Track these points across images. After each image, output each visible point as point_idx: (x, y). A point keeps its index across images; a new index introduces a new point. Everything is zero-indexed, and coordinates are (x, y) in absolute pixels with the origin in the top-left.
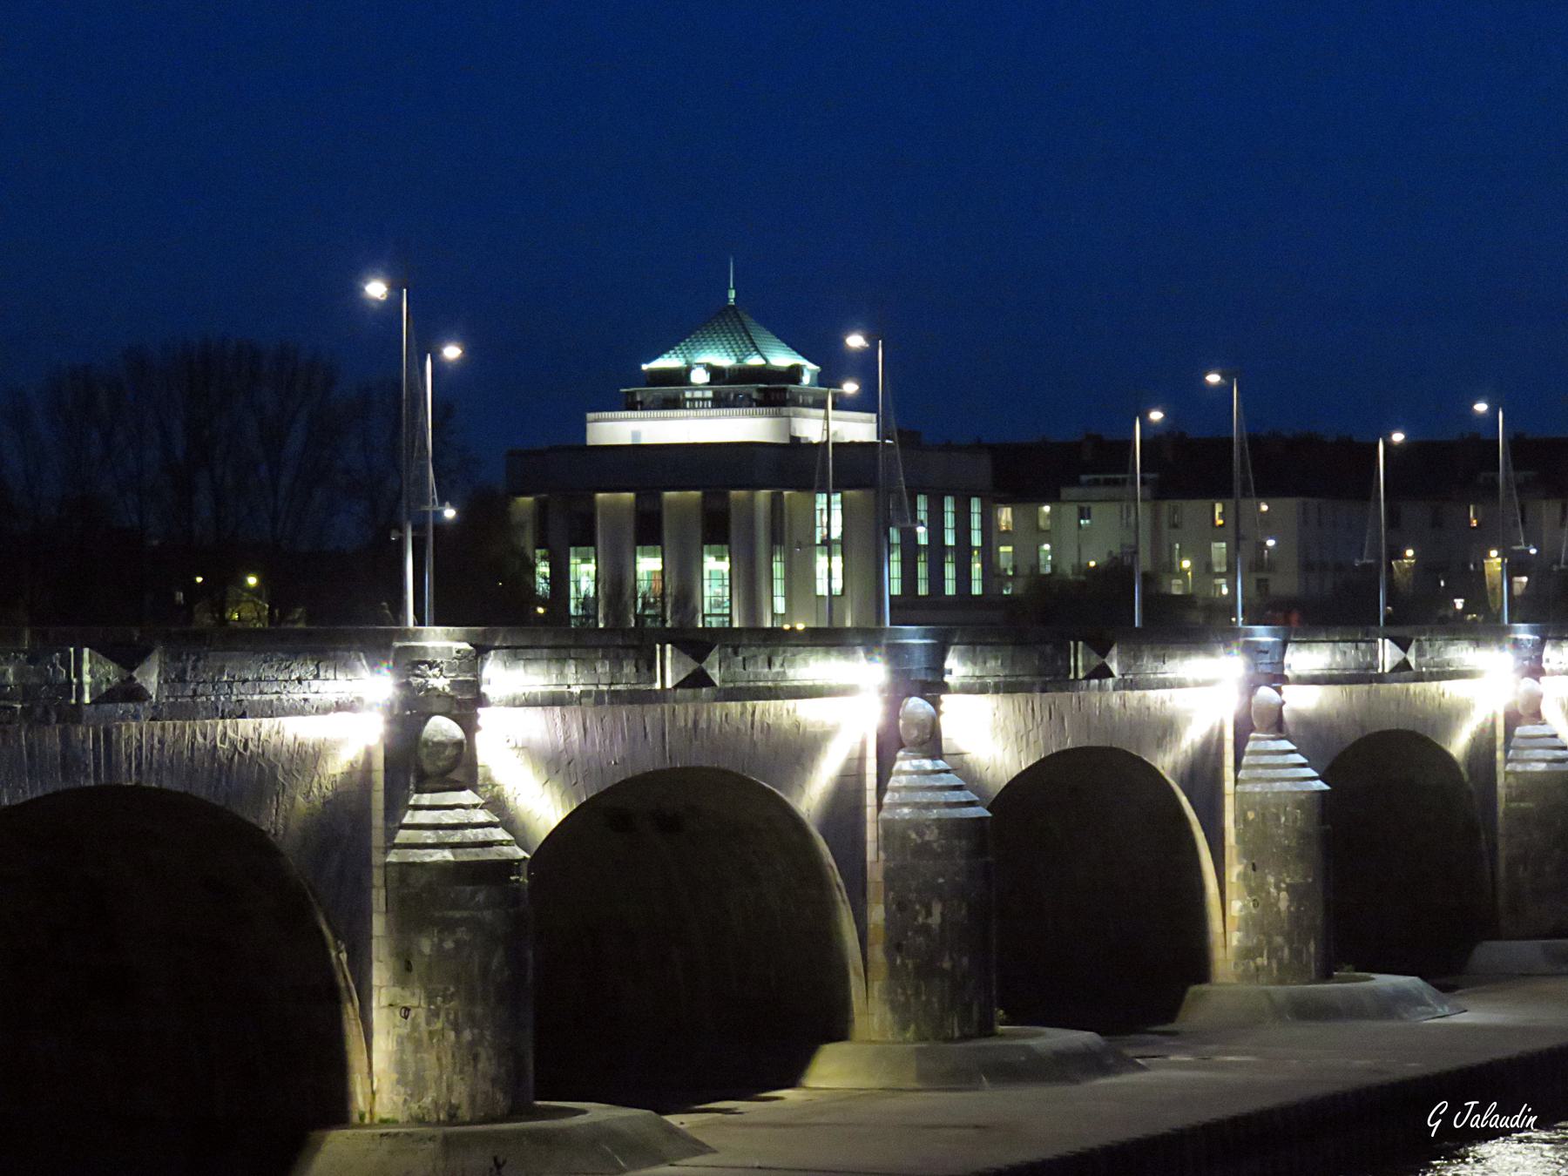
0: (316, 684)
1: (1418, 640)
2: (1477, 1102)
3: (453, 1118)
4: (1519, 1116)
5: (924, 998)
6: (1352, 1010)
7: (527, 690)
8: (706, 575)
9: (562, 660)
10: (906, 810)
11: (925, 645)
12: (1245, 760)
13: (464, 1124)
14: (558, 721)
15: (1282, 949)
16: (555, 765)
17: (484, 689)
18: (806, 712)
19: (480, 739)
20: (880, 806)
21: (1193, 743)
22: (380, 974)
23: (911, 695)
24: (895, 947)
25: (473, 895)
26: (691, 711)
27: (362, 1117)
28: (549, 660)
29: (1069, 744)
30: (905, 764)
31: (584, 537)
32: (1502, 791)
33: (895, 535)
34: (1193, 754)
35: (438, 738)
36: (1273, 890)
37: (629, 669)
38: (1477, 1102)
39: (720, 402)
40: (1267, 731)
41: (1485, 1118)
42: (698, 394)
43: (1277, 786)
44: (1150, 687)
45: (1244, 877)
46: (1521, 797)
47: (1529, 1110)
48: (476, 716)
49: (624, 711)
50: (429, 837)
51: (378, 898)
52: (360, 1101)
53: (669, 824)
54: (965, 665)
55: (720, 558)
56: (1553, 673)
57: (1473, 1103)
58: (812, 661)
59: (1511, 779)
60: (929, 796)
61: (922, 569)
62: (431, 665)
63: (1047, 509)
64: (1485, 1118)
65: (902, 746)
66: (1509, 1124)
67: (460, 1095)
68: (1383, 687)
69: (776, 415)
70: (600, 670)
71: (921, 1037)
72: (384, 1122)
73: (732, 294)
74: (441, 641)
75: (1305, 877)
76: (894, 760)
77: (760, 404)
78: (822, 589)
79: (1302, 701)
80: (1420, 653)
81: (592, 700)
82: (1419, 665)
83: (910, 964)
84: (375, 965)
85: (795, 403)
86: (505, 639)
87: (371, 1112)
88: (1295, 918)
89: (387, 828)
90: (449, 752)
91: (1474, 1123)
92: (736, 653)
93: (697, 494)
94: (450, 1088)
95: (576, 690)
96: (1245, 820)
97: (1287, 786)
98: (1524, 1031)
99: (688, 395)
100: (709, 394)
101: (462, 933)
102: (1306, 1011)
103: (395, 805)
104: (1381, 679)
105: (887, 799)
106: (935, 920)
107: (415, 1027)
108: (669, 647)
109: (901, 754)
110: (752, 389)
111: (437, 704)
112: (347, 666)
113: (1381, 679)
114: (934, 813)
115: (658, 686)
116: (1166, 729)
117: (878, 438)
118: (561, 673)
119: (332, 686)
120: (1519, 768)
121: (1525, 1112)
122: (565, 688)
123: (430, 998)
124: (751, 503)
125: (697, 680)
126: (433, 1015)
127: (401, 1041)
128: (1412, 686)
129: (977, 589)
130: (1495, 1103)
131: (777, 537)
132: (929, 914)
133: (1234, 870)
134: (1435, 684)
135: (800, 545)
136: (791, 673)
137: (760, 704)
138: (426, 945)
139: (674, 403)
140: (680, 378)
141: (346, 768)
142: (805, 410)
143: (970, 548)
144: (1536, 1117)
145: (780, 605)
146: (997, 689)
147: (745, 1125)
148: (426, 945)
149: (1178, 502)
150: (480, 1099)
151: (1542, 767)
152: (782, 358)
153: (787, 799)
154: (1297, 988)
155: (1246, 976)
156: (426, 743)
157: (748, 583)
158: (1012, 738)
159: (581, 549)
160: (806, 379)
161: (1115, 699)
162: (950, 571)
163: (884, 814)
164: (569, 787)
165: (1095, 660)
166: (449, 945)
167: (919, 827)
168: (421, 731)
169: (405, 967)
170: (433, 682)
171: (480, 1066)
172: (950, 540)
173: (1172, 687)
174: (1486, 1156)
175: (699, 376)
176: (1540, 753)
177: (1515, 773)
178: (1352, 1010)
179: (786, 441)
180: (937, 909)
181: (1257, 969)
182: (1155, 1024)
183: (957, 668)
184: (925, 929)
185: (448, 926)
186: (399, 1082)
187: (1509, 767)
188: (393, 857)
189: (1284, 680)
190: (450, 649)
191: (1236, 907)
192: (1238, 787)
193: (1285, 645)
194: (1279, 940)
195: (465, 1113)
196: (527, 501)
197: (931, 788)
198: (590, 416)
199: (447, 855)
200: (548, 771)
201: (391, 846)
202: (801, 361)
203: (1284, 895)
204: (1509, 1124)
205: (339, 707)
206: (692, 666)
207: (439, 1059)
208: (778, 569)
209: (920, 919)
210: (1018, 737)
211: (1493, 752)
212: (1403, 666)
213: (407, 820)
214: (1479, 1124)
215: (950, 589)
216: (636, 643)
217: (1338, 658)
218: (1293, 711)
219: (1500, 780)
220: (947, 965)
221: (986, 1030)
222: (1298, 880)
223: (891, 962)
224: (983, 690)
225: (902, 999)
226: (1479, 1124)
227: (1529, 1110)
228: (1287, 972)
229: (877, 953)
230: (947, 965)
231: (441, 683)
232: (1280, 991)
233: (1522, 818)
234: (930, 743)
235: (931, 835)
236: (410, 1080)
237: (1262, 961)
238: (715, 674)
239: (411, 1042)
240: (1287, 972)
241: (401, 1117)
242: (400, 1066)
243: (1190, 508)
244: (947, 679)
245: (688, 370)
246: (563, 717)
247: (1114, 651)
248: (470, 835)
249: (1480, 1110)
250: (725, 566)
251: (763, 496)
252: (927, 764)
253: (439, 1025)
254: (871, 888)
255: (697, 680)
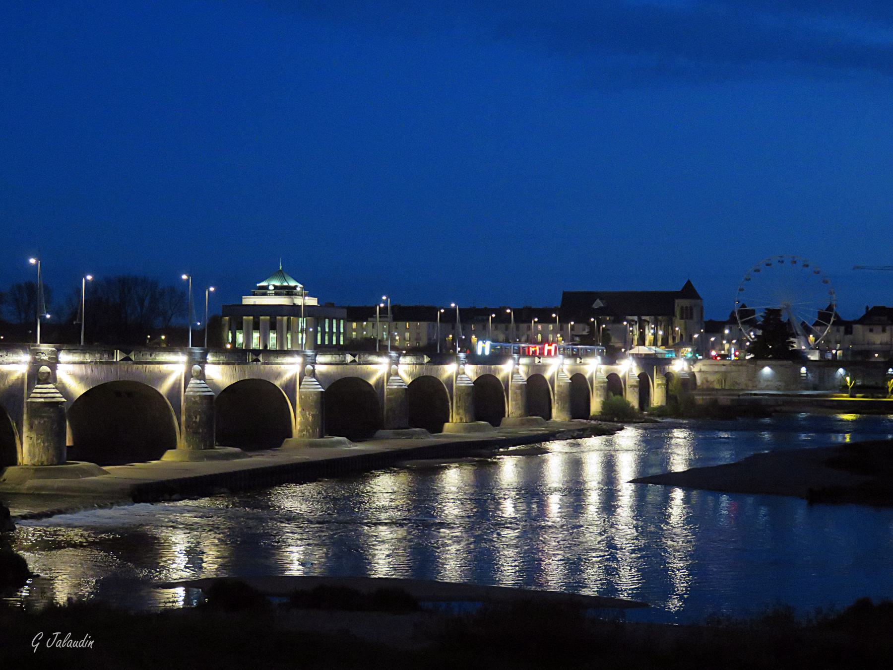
0: (6, 357)
1: (360, 355)
2: (60, 633)
3: (42, 465)
4: (84, 641)
5: (194, 439)
6: (325, 445)
7: (73, 360)
8: (270, 338)
9: (85, 353)
10: (191, 393)
11: (200, 352)
12: (302, 383)
13: (45, 466)
14: (84, 369)
15: (309, 430)
16: (82, 379)
17: (59, 360)
18: (163, 368)
19: (57, 372)
20: (185, 392)
21: (287, 379)
22: (25, 429)
23: (195, 365)
24: (188, 427)
25: (49, 410)
26: (126, 367)
27: (20, 464)
28: (81, 353)
29: (247, 378)
30: (193, 381)
31: (240, 328)
32: (385, 393)
33: (319, 329)
34: (287, 381)
35: (43, 371)
36: (308, 415)
37: (106, 356)
38: (60, 633)
39: (276, 294)
40: (310, 376)
41: (64, 642)
42: (271, 292)
43: (310, 390)
44: (272, 365)
45: (301, 412)
46: (391, 394)
47: (90, 637)
48: (57, 366)
49: (105, 366)
50: (39, 395)
51: (25, 410)
52: (20, 460)
53: (129, 394)
54: (213, 357)
55: (274, 333)
56: (402, 364)
57: (57, 633)
58: (164, 355)
59: (388, 390)
60: (198, 389)
61: (327, 338)
62: (42, 353)
63: (365, 323)
64: (64, 642)
65: (192, 377)
66: (78, 645)
67: (44, 458)
68: (348, 366)
69: (290, 298)
70: (96, 356)
71: (193, 448)
72: (26, 465)
73: (281, 267)
74: (46, 348)
75: (316, 412)
76: (190, 380)
77: (286, 295)
78: (300, 342)
79: (319, 369)
80: (359, 358)
81: (94, 363)
82: (359, 361)
83: (191, 430)
84: (24, 427)
85: (296, 295)
86: (66, 347)
87: (22, 463)
88: (313, 422)
89: (27, 393)
90: (46, 375)
91: (58, 645)
92: (140, 353)
93: (268, 317)
94: (41, 457)
95: (89, 361)
96: (302, 398)
97: (312, 390)
98: (363, 451)
99: (268, 292)
100: (274, 292)
101: (46, 419)
102: (312, 445)
103: (30, 387)
104: (347, 364)
105: (187, 390)
106: (198, 420)
107: (33, 442)
108: (118, 351)
109: (192, 379)
110: (284, 291)
111: (44, 363)
112: (16, 353)
113: (347, 364)
114: (198, 394)
115: (115, 360)
116: (278, 375)
117: (318, 304)
118: (84, 356)
119: (12, 357)
120: (390, 387)
121: (87, 639)
122: (86, 360)
123: (37, 435)
124: (282, 321)
125: (127, 359)
126: (37, 439)
127: (30, 445)
128: (358, 366)
129: (342, 343)
130: (70, 634)
131: (289, 329)
132: (196, 418)
133: (298, 410)
134: (365, 366)
135: (295, 332)
136: (157, 358)
137: (148, 366)
138: (36, 422)
139: (265, 294)
140: (266, 288)
141: (16, 378)
142: (297, 297)
143: (333, 333)
144: (93, 641)
145: (289, 346)
146: (223, 364)
147: (137, 469)
148: (36, 422)
149: (397, 322)
150: (49, 460)
151: (396, 387)
152: (292, 283)
153: (156, 389)
154: (311, 440)
155: (301, 437)
156: (40, 373)
157: (281, 339)
158: (229, 376)
159: (240, 331)
160: (298, 289)
161: (262, 367)
162: (334, 338)
163: (186, 394)
164: (86, 384)
165: (254, 357)
166: (42, 422)
167: (194, 397)
168: (38, 370)
169: (31, 427)
170: (42, 358)
171: (50, 452)
172: (335, 330)
173: (279, 364)
174: (622, 505)
175: (271, 288)
176: (396, 384)
177: (389, 389)
178: (325, 445)
179: (292, 304)
180: (198, 417)
181: (304, 435)
182: (274, 447)
183: (210, 358)
184: (195, 422)
185: (42, 417)
186: (29, 455)
187: (388, 387)
188: (29, 400)
189: (316, 363)
190: (48, 350)
191: (298, 419)
192: (300, 390)
193: (316, 355)
194: (309, 428)
195: (45, 463)
196: (227, 318)
197: (198, 388)
198: (243, 297)
199: (42, 400)
200: (80, 380)
201: (29, 397)
202: (297, 284)
203: (310, 417)
204: (78, 645)
205: (13, 363)
206: (125, 355)
207: (39, 450)
208: (289, 336)
209: (194, 420)
210: (230, 376)
211: (383, 383)
212: (354, 361)
213: (34, 391)
214: (61, 645)
215: (334, 343)
216: (108, 349)
217: (334, 359)
218: (319, 372)
219: (385, 390)
220: (201, 431)
221: (212, 447)
222: (314, 413)
223: (187, 431)
224: (219, 364)
225: (189, 439)
226: (61, 645)
227: (90, 637)
228: (313, 435)
229: (183, 428)
230: (201, 431)
231: (45, 358)
232: (307, 440)
233: (389, 400)
234: (201, 375)
235: (197, 399)
236: (32, 455)
237: (305, 433)
238: (133, 358)
239: (32, 446)
240: (313, 435)
241: (29, 464)
242: (29, 452)
243: (400, 324)
244: (207, 361)
245: (269, 286)
246: (85, 367)
247: (261, 355)
248: (49, 395)
249: (61, 637)
250: (275, 335)
251: (285, 318)
252: (198, 382)
253: (39, 441)
254: (182, 412)
255: (127, 359)
